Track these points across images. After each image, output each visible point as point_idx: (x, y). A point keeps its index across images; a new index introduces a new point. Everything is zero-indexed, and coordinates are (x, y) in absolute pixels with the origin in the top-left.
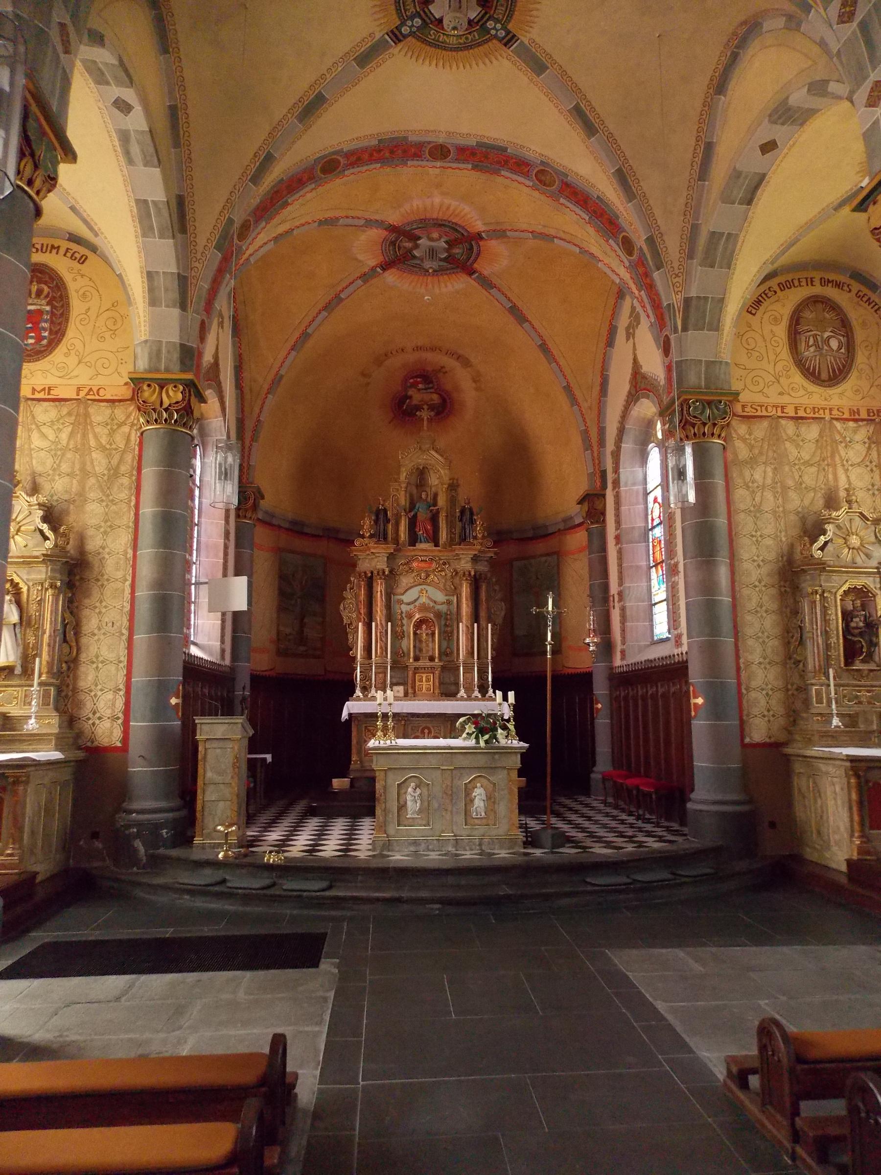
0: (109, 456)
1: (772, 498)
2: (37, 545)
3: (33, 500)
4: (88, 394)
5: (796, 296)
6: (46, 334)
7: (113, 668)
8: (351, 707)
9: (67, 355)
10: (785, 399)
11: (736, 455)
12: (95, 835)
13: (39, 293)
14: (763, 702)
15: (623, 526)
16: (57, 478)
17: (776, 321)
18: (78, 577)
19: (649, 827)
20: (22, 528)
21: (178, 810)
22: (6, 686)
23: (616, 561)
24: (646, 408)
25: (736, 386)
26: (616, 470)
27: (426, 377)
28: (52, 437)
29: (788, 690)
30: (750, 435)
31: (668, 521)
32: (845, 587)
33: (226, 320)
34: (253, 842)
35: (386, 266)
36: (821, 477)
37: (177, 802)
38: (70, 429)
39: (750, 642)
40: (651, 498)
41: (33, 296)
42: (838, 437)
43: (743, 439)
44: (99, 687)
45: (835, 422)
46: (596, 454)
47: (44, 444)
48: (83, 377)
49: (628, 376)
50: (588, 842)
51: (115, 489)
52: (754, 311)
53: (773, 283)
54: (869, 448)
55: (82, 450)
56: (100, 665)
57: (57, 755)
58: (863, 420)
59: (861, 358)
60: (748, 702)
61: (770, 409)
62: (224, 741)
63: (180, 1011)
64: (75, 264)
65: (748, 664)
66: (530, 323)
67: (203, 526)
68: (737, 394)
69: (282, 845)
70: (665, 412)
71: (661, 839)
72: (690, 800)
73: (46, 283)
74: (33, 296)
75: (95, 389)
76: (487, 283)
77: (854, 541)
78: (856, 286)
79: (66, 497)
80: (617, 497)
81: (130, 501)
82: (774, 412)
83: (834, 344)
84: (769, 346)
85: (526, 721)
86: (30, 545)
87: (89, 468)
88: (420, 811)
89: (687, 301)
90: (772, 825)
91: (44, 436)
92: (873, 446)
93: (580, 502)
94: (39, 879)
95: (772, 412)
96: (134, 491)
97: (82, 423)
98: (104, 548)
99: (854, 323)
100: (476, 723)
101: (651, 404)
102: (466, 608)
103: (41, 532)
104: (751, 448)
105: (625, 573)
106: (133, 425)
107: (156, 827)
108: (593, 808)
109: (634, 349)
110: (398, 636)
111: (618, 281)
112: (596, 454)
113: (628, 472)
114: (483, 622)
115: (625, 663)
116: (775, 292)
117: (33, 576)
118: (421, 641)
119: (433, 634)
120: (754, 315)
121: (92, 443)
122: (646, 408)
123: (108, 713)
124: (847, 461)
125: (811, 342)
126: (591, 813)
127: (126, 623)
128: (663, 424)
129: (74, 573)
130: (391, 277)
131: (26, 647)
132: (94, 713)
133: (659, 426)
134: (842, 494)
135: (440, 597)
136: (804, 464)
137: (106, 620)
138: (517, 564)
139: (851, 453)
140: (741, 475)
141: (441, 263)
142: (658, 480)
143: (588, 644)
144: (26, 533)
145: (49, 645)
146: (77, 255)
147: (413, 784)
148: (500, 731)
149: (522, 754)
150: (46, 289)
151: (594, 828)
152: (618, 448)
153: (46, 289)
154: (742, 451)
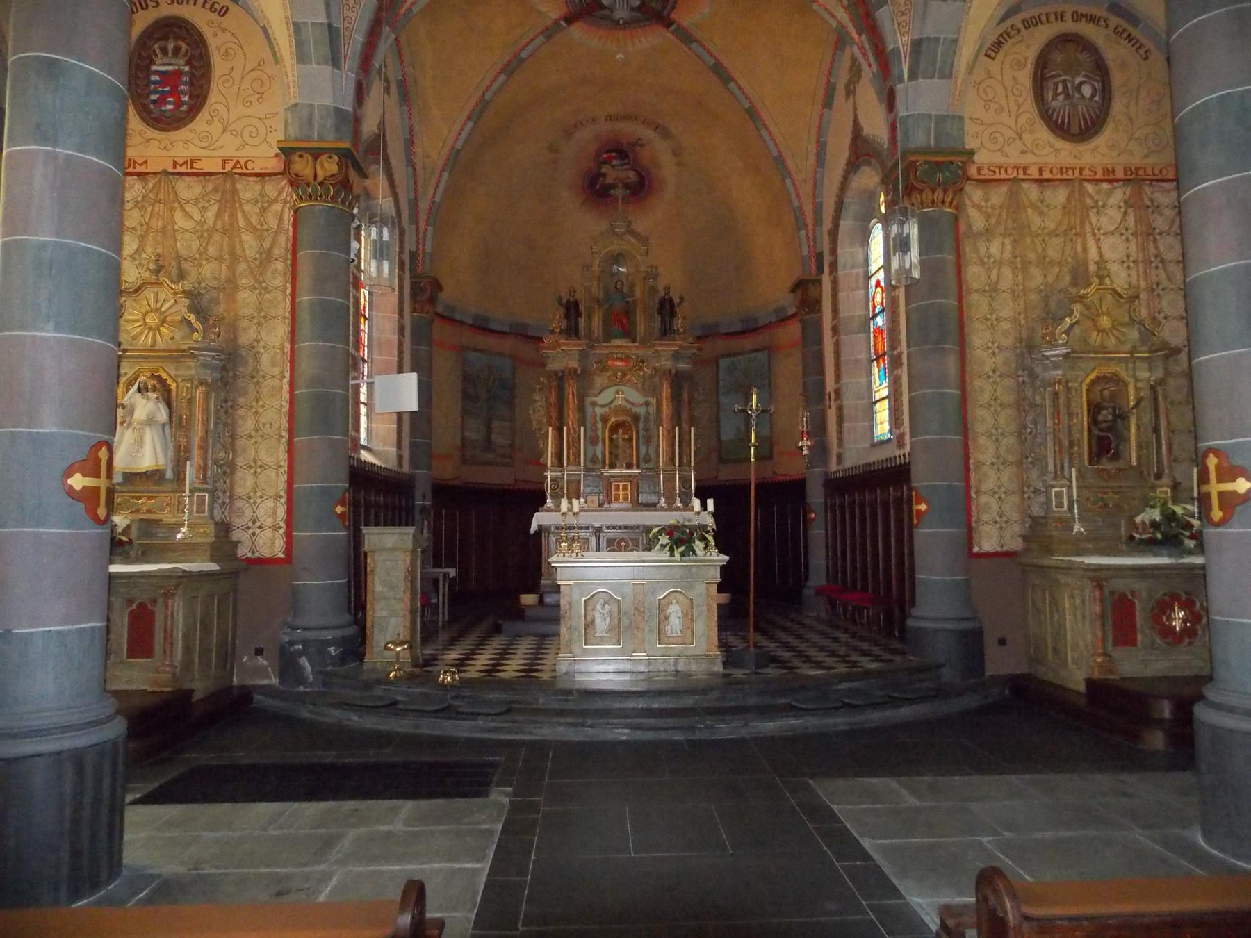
0: (260, 238)
1: (1010, 275)
2: (184, 338)
3: (179, 287)
4: (234, 167)
5: (1044, 33)
6: (186, 99)
7: (272, 473)
8: (540, 519)
9: (210, 123)
10: (1029, 159)
11: (970, 226)
12: (259, 652)
13: (177, 51)
14: (995, 507)
15: (841, 315)
16: (204, 262)
17: (1019, 65)
18: (231, 374)
19: (865, 646)
20: (169, 319)
21: (349, 625)
22: (159, 492)
23: (832, 355)
24: (868, 178)
25: (970, 144)
26: (834, 252)
27: (620, 150)
28: (197, 216)
29: (1023, 492)
30: (987, 201)
31: (891, 308)
32: (1093, 376)
33: (393, 87)
34: (430, 661)
35: (570, 19)
36: (1068, 249)
37: (347, 618)
38: (216, 207)
39: (982, 440)
40: (873, 282)
41: (170, 54)
42: (1088, 201)
43: (979, 207)
44: (259, 494)
45: (1086, 184)
46: (810, 234)
47: (189, 225)
48: (229, 148)
49: (847, 141)
50: (796, 662)
51: (269, 274)
52: (993, 54)
53: (1017, 20)
54: (1125, 213)
55: (230, 231)
56: (259, 470)
57: (212, 566)
58: (1118, 180)
59: (1117, 107)
60: (977, 506)
61: (1010, 171)
62: (393, 552)
63: (329, 843)
64: (215, 17)
65: (979, 465)
66: (736, 83)
67: (374, 321)
68: (972, 153)
69: (461, 664)
70: (888, 181)
71: (877, 659)
72: (910, 616)
73: (184, 40)
74: (170, 54)
75: (242, 161)
76: (686, 37)
77: (1105, 322)
78: (1114, 21)
79: (215, 284)
80: (835, 283)
81: (285, 289)
82: (1015, 175)
83: (1087, 91)
84: (1010, 94)
85: (728, 535)
86: (178, 337)
87: (239, 252)
88: (610, 629)
89: (917, 45)
90: (1002, 642)
91: (188, 216)
92: (1129, 210)
93: (793, 290)
94: (197, 697)
95: (1012, 174)
96: (289, 276)
97: (229, 200)
98: (258, 342)
99: (1111, 64)
100: (670, 534)
101: (873, 173)
102: (666, 410)
103: (189, 322)
104: (988, 217)
105: (843, 369)
106: (285, 202)
107: (325, 643)
108: (804, 626)
109: (855, 109)
110: (593, 441)
111: (835, 25)
112: (810, 234)
113: (846, 253)
114: (685, 426)
115: (841, 467)
116: (1019, 31)
117: (181, 372)
118: (617, 447)
119: (631, 439)
120: (993, 59)
121: (242, 223)
122: (868, 178)
123: (269, 522)
124: (1099, 229)
125: (1060, 89)
126: (801, 631)
127: (285, 425)
128: (886, 195)
129: (228, 369)
130: (577, 31)
131: (178, 448)
132: (254, 522)
133: (882, 198)
134: (1092, 268)
135: (637, 397)
136: (1049, 234)
137: (264, 421)
138: (724, 363)
139: (1104, 220)
140: (977, 250)
141: (634, 14)
142: (881, 262)
143: (801, 448)
144: (173, 324)
145: (201, 447)
146: (216, 6)
147: (602, 601)
148: (697, 542)
149: (722, 567)
150: (184, 46)
151: (803, 647)
152: (836, 225)
153: (184, 46)
154: (976, 219)
